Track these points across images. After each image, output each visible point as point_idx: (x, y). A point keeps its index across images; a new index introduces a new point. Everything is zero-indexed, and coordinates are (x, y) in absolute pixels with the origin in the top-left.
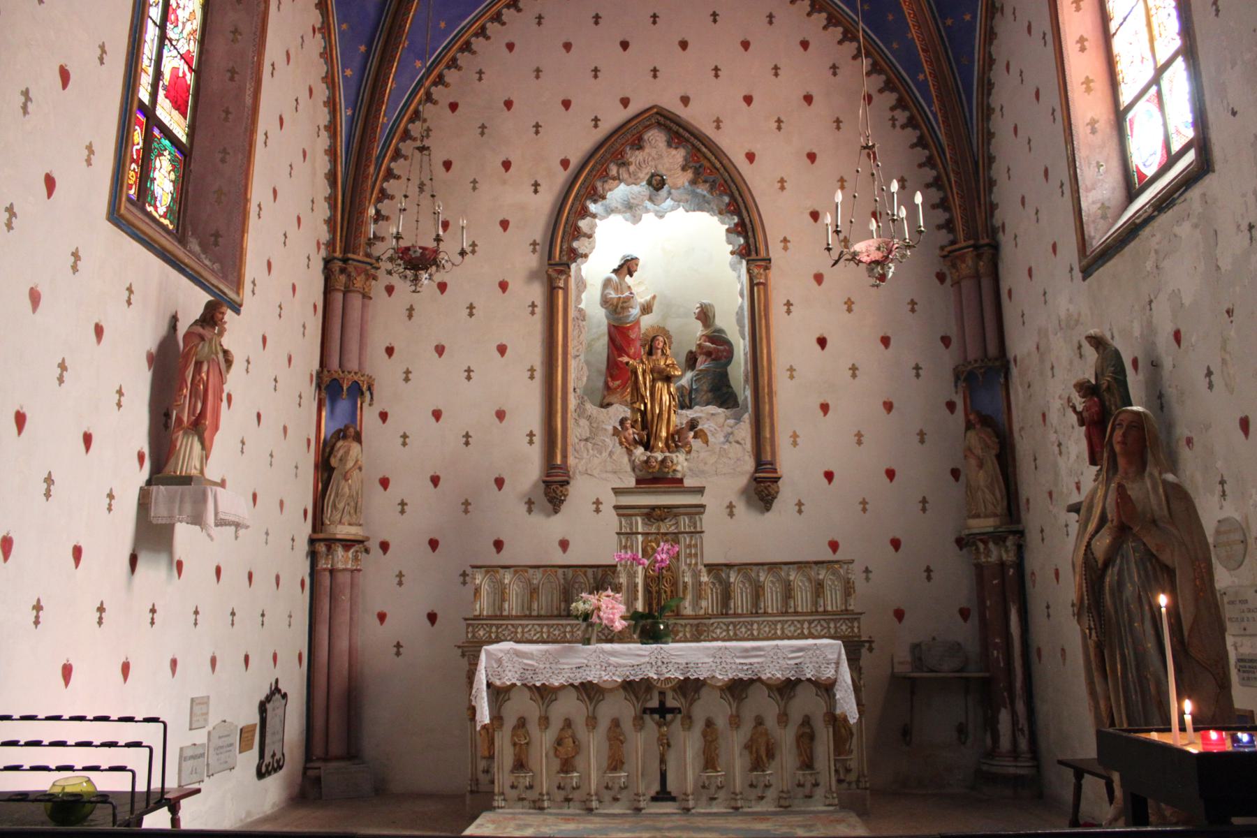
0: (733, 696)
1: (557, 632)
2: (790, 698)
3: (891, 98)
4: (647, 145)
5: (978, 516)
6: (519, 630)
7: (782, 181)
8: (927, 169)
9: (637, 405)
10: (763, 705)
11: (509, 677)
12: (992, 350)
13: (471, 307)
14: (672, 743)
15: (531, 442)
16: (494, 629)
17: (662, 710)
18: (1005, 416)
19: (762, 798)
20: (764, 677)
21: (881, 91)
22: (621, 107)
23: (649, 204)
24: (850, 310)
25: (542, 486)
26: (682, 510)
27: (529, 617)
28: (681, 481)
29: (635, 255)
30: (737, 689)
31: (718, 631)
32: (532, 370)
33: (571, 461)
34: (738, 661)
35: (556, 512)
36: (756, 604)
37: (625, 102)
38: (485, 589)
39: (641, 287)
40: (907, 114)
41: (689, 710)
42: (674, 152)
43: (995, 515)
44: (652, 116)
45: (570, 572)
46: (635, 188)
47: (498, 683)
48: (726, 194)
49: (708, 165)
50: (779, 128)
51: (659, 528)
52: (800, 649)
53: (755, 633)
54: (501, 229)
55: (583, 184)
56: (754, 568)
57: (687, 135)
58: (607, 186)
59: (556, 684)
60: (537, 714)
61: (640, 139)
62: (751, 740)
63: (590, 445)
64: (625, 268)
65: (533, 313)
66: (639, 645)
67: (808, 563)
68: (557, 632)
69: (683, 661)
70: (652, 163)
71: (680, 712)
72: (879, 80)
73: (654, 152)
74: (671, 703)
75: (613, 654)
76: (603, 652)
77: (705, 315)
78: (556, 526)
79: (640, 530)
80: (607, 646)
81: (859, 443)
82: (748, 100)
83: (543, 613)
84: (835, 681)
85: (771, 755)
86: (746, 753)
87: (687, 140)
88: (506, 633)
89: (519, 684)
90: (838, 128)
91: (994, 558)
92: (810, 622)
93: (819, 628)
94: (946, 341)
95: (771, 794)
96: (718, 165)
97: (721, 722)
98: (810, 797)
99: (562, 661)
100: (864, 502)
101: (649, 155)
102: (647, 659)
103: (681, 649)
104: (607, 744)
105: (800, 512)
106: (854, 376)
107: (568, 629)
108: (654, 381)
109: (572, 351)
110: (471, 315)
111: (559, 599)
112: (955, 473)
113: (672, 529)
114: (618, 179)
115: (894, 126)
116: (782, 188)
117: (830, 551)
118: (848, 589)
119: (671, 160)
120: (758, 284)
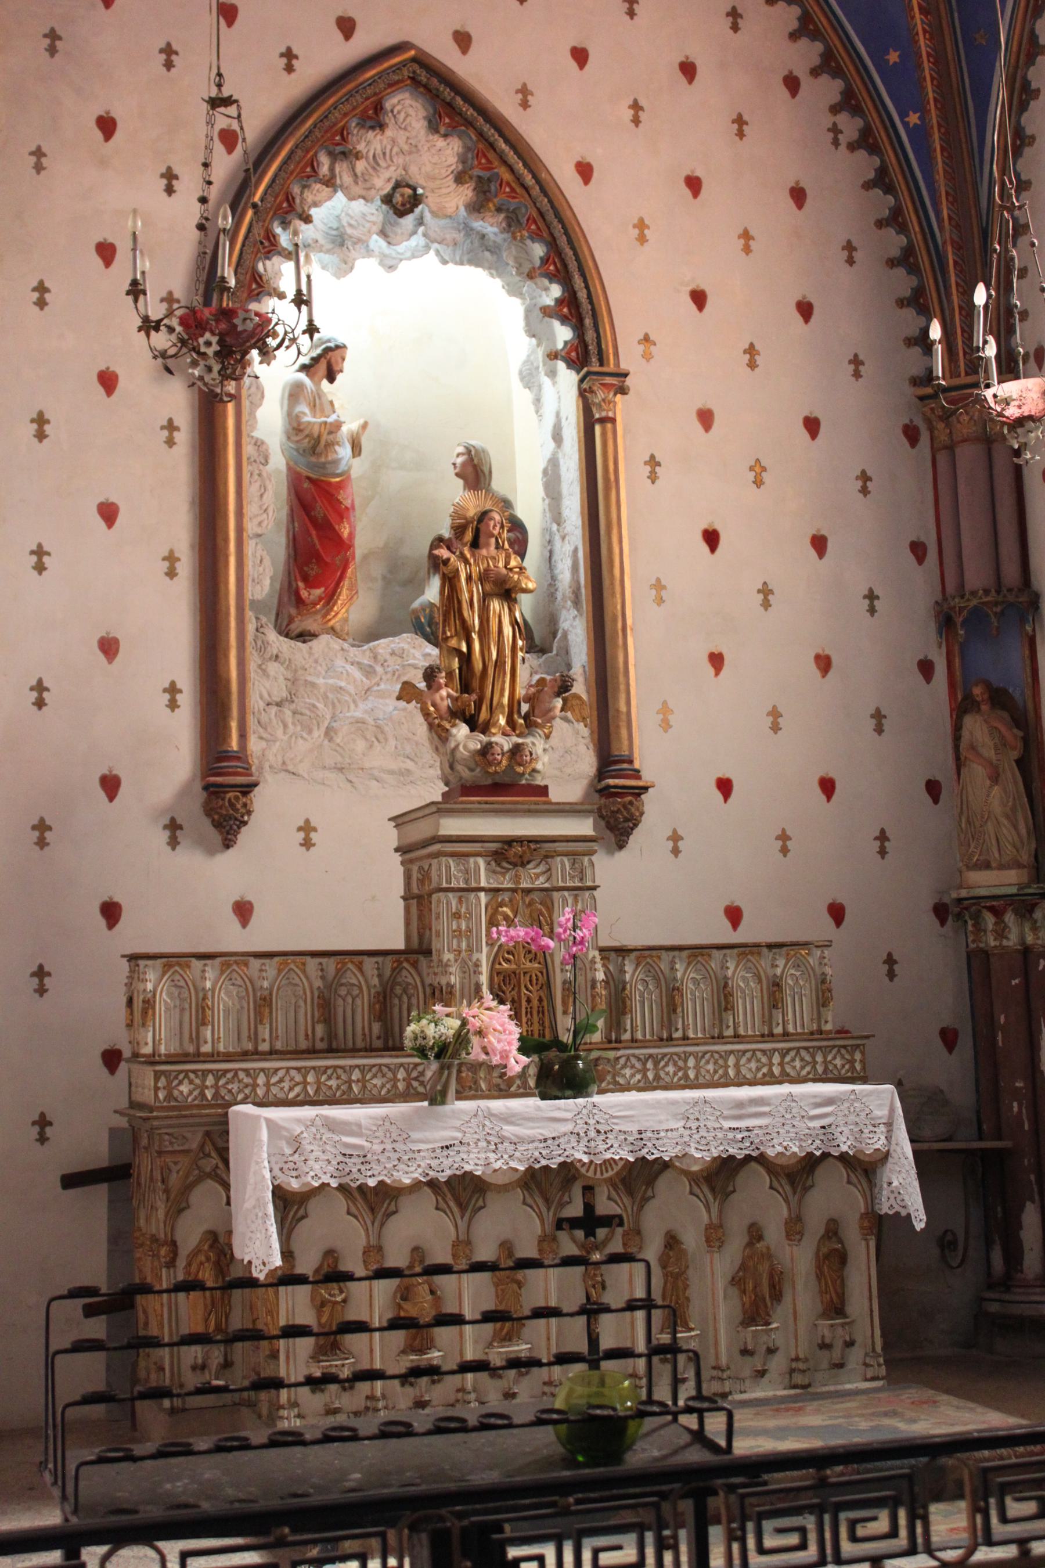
0: (713, 1190)
1: (333, 1083)
2: (806, 1189)
3: (830, 89)
4: (389, 119)
5: (987, 866)
6: (261, 1080)
7: (641, 225)
8: (891, 232)
9: (453, 643)
10: (760, 1202)
11: (318, 1171)
12: (1011, 572)
13: (41, 420)
14: (608, 1283)
15: (173, 705)
16: (210, 1080)
17: (590, 1222)
18: (1029, 693)
19: (762, 1373)
20: (771, 1153)
21: (815, 72)
22: (339, 36)
23: (377, 242)
24: (758, 483)
25: (200, 796)
26: (561, 847)
27: (255, 1054)
28: (543, 791)
29: (341, 340)
30: (722, 1175)
31: (628, 1072)
32: (171, 558)
33: (254, 745)
34: (727, 1124)
35: (228, 844)
36: (668, 1023)
37: (347, 27)
38: (163, 1000)
39: (348, 399)
40: (859, 123)
41: (637, 1221)
42: (441, 143)
43: (1019, 866)
44: (404, 64)
45: (330, 964)
46: (358, 206)
47: (295, 1185)
48: (536, 236)
49: (506, 176)
50: (636, 121)
51: (517, 879)
52: (829, 1101)
53: (692, 1074)
54: (99, 262)
55: (270, 186)
56: (715, 953)
57: (471, 112)
58: (309, 196)
59: (407, 1181)
60: (362, 1242)
61: (378, 108)
62: (743, 1267)
63: (288, 713)
64: (322, 367)
65: (170, 442)
66: (534, 1102)
67: (757, 945)
68: (333, 1083)
69: (634, 1128)
70: (400, 160)
71: (621, 1224)
72: (809, 52)
73: (401, 137)
74: (604, 1206)
75: (508, 1119)
76: (490, 1115)
77: (474, 471)
78: (228, 872)
79: (483, 884)
80: (498, 1105)
81: (776, 728)
82: (580, 56)
83: (279, 1045)
84: (887, 1155)
85: (777, 1296)
86: (734, 1292)
87: (469, 123)
88: (234, 1087)
89: (334, 1184)
90: (741, 134)
91: (1012, 940)
92: (784, 1053)
93: (798, 1064)
94: (918, 550)
95: (777, 1364)
96: (529, 180)
97: (692, 1239)
98: (841, 1366)
99: (415, 1135)
100: (784, 837)
101: (393, 141)
102: (569, 1127)
103: (629, 1106)
104: (493, 1289)
105: (676, 851)
106: (766, 605)
107: (356, 1075)
108: (485, 597)
109: (251, 527)
110: (41, 436)
111: (361, 1018)
112: (933, 789)
113: (541, 882)
114: (330, 182)
115: (836, 143)
116: (642, 239)
117: (727, 924)
118: (823, 997)
119: (434, 158)
120: (603, 421)
